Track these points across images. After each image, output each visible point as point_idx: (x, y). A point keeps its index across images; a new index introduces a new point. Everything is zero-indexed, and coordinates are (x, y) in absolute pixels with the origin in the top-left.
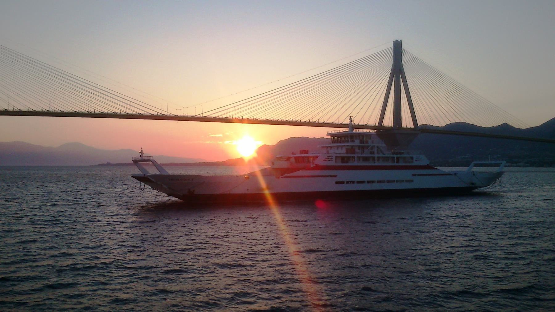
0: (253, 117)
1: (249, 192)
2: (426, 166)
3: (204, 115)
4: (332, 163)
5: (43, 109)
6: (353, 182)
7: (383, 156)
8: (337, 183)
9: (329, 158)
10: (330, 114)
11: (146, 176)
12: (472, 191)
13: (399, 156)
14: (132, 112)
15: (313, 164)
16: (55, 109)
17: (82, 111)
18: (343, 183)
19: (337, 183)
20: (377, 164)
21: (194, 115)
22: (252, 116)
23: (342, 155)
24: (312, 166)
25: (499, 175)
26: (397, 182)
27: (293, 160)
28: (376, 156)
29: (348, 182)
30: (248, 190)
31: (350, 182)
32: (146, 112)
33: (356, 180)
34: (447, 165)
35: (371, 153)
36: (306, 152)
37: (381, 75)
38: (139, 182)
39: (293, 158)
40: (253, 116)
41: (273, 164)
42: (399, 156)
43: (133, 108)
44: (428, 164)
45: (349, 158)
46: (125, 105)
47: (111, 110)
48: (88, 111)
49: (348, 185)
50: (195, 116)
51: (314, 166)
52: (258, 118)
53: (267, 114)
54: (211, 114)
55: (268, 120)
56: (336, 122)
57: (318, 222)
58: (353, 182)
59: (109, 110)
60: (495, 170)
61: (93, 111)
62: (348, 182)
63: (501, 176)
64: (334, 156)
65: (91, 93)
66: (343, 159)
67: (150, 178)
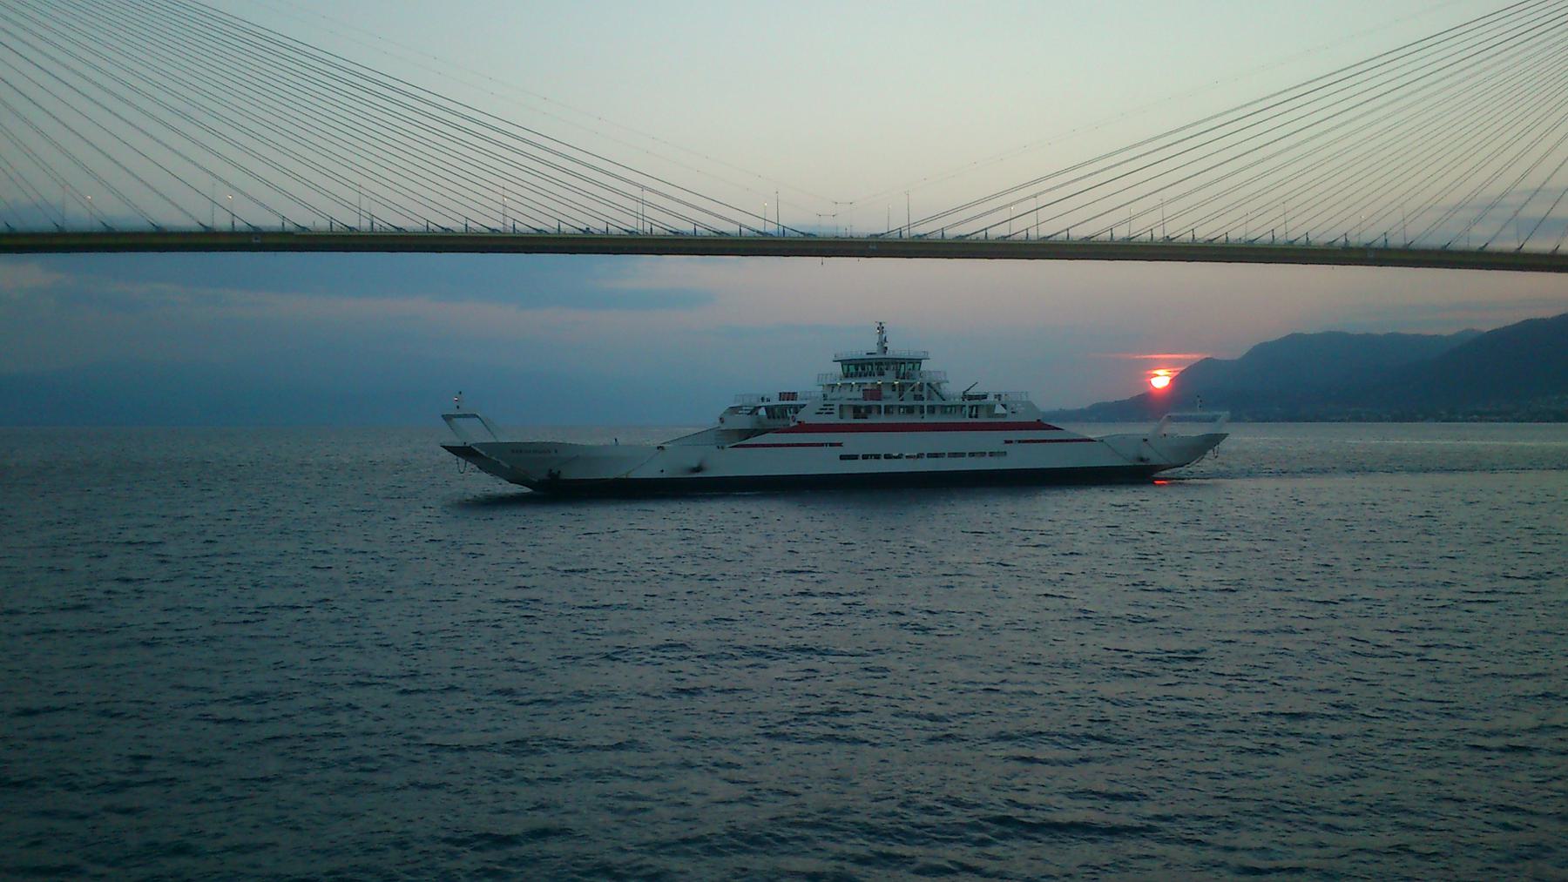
0: (1151, 230)
1: (664, 475)
2: (1035, 423)
3: (920, 230)
4: (833, 419)
5: (470, 224)
6: (877, 457)
7: (943, 403)
8: (842, 458)
9: (827, 409)
11: (468, 445)
12: (529, 490)
13: (976, 402)
14: (781, 229)
15: (794, 421)
17: (562, 230)
18: (857, 459)
19: (842, 458)
20: (928, 419)
21: (1008, 234)
22: (1187, 230)
23: (855, 403)
24: (792, 424)
25: (1213, 441)
26: (991, 456)
27: (762, 412)
28: (926, 403)
29: (865, 457)
30: (662, 471)
31: (871, 455)
32: (745, 227)
33: (967, 451)
34: (1420, 416)
35: (916, 398)
36: (793, 396)
37: (183, 90)
38: (455, 457)
39: (763, 409)
40: (1191, 228)
41: (722, 420)
42: (976, 402)
43: (649, 212)
44: (1039, 420)
45: (869, 409)
46: (636, 192)
47: (661, 225)
48: (539, 226)
49: (992, 458)
50: (1010, 236)
51: (796, 424)
52: (1212, 237)
53: (1289, 216)
54: (1066, 227)
56: (1461, 244)
57: (1254, 519)
58: (877, 457)
59: (658, 224)
60: (1195, 431)
61: (647, 228)
62: (865, 457)
63: (1218, 443)
64: (837, 404)
65: (458, 128)
66: (856, 410)
67: (478, 450)
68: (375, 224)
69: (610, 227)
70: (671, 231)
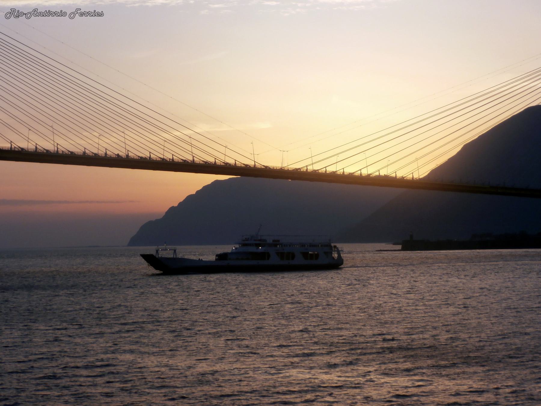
10: (334, 160)
16: (37, 146)
48: (141, 155)
52: (404, 176)
55: (405, 178)
68: (59, 149)
69: (256, 164)
70: (203, 161)
